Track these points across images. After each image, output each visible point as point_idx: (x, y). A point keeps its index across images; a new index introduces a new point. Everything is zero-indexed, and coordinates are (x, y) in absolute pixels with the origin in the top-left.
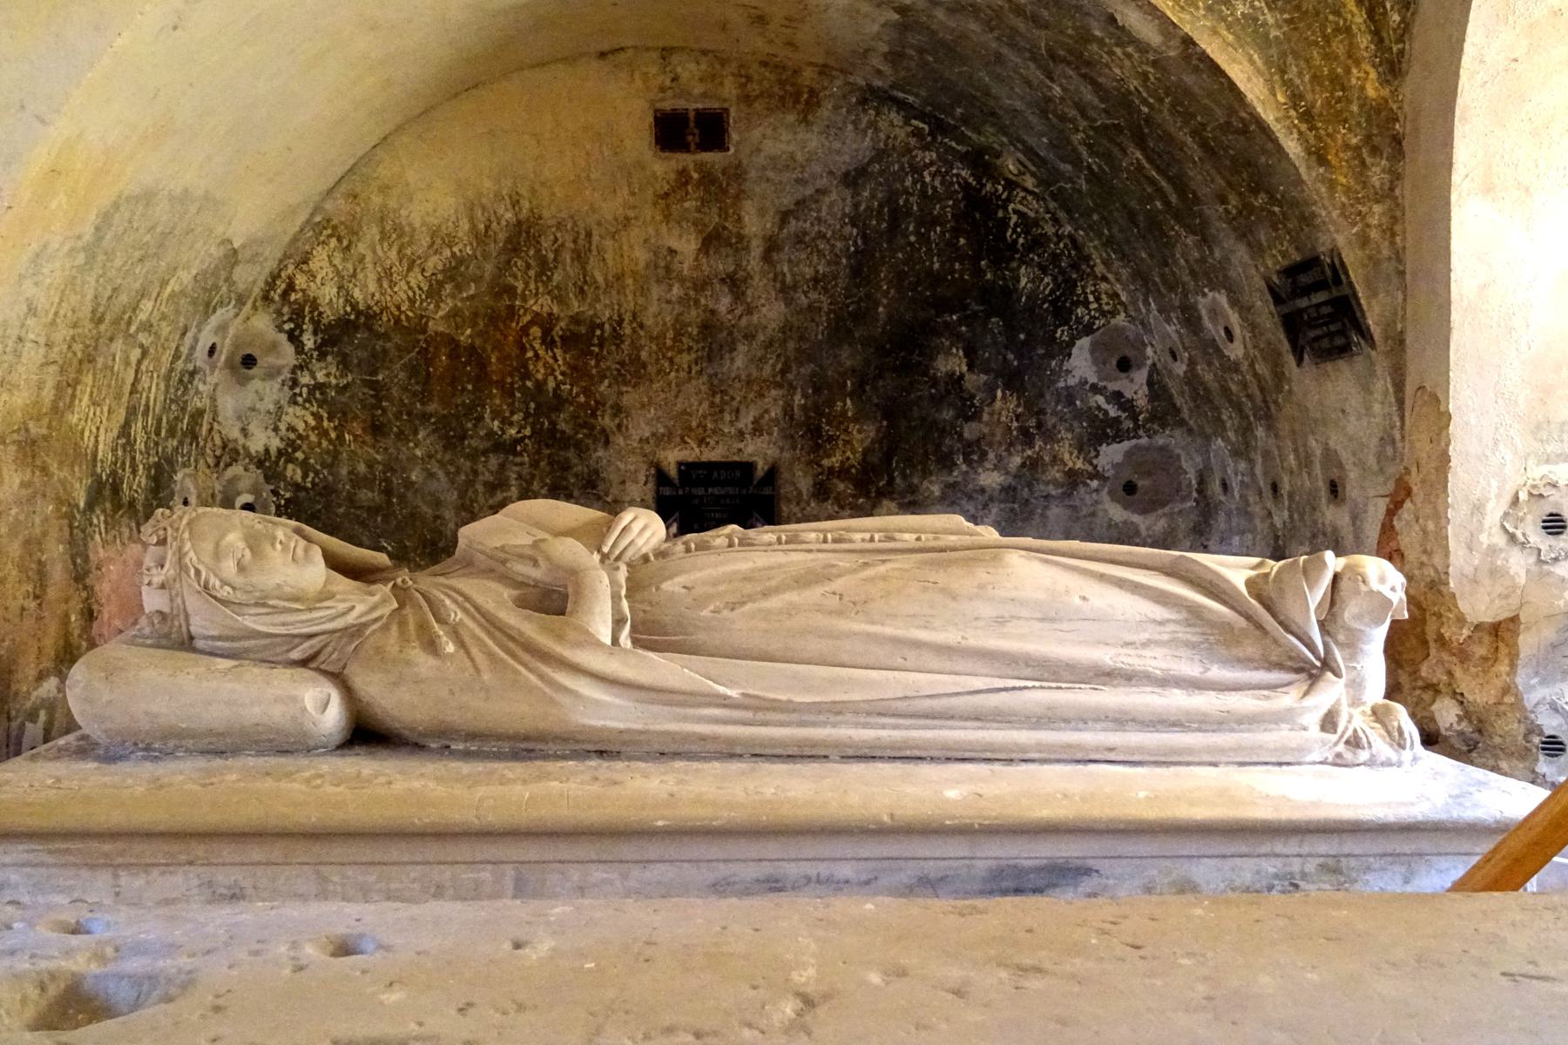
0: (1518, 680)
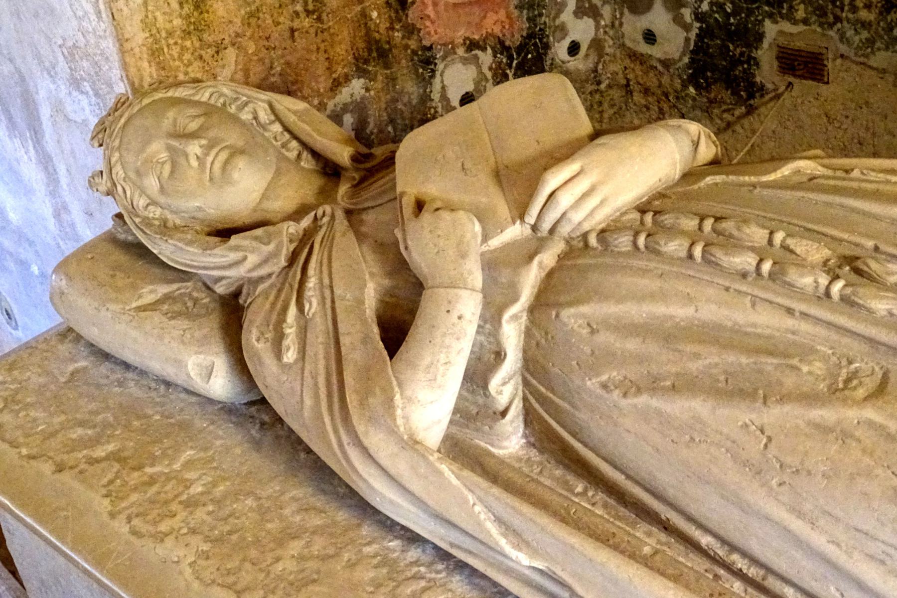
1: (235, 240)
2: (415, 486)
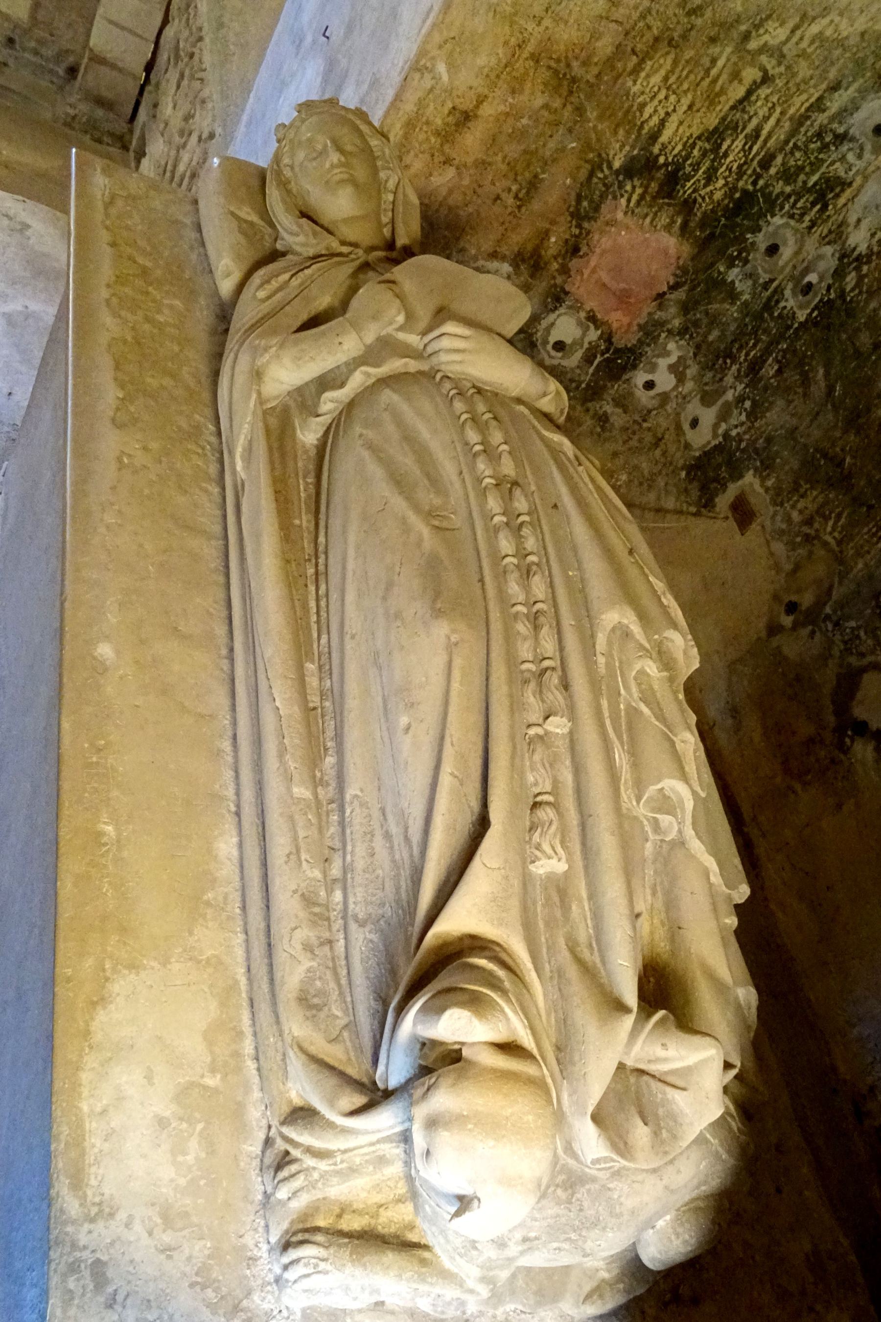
1: (304, 221)
2: (236, 395)
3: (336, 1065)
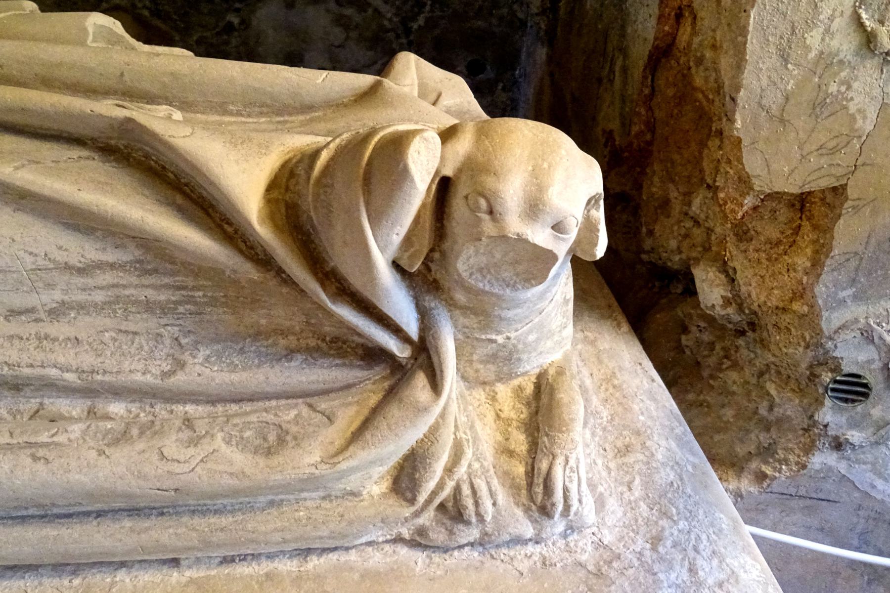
0: (820, 289)
3: (362, 418)
